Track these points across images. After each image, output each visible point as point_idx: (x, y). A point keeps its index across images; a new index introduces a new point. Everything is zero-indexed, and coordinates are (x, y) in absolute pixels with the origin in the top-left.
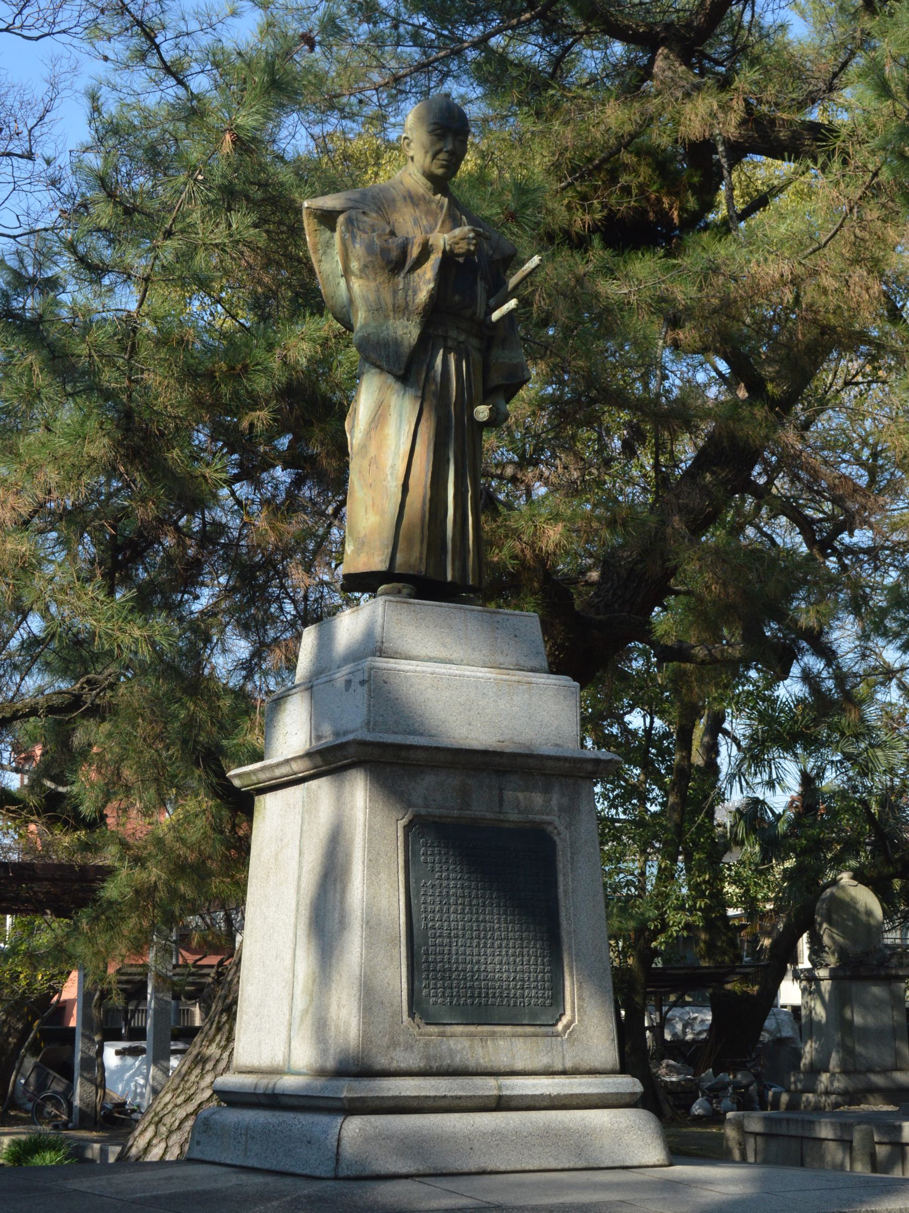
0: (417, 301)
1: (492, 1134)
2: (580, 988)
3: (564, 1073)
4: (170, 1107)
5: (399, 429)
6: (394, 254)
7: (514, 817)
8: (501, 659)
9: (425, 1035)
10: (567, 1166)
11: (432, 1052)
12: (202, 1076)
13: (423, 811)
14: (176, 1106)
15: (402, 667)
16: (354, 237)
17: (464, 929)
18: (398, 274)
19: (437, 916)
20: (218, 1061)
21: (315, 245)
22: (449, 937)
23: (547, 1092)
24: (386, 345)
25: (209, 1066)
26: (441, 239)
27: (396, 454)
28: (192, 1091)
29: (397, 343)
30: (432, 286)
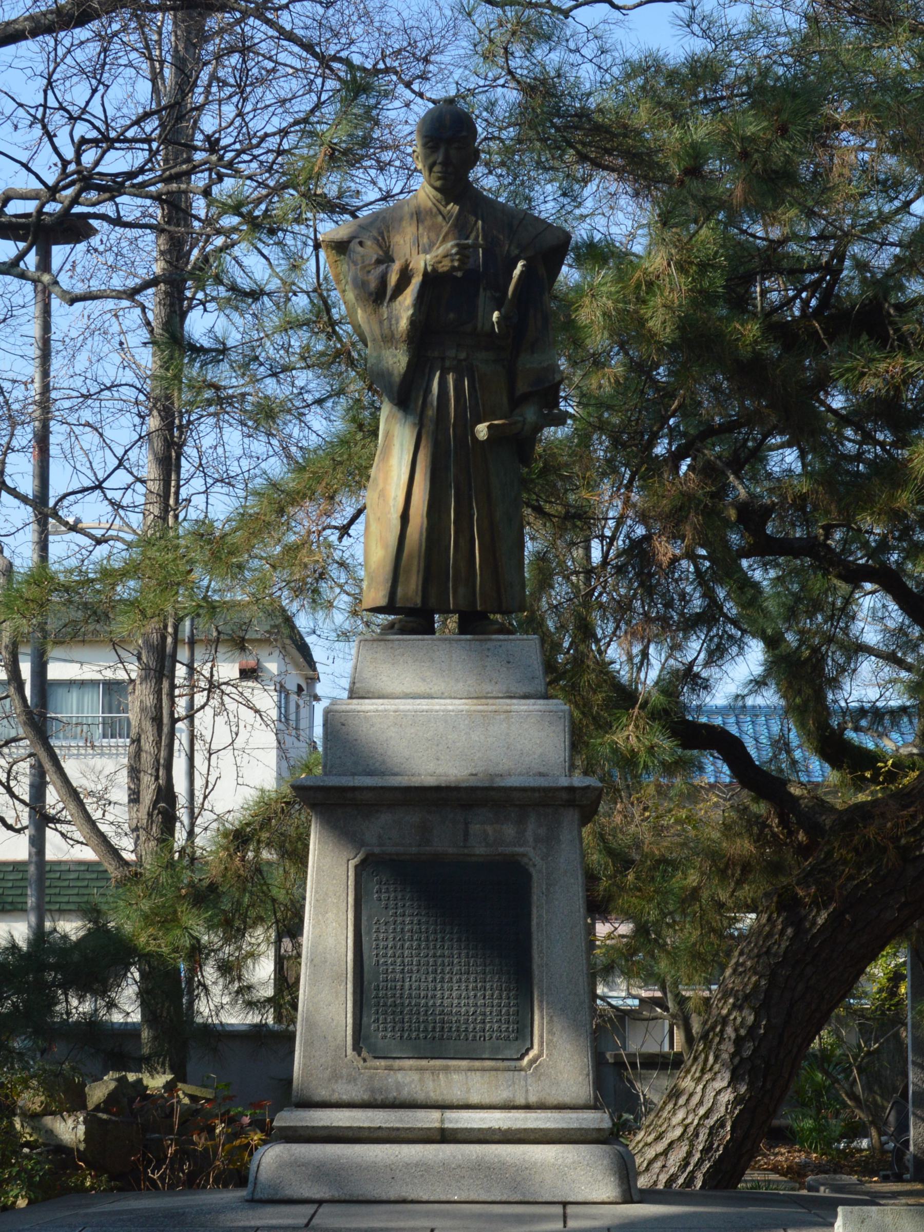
0: (400, 329)
1: (417, 1165)
2: (551, 1021)
3: (527, 1107)
4: (641, 1145)
5: (401, 459)
6: (373, 285)
7: (480, 850)
8: (488, 688)
9: (370, 1068)
10: (498, 1199)
11: (377, 1084)
12: (674, 1112)
13: (377, 850)
14: (646, 1144)
15: (363, 708)
17: (419, 965)
18: (382, 303)
19: (390, 952)
20: (691, 1095)
22: (402, 971)
23: (496, 1126)
25: (682, 1101)
28: (663, 1129)
30: (411, 312)
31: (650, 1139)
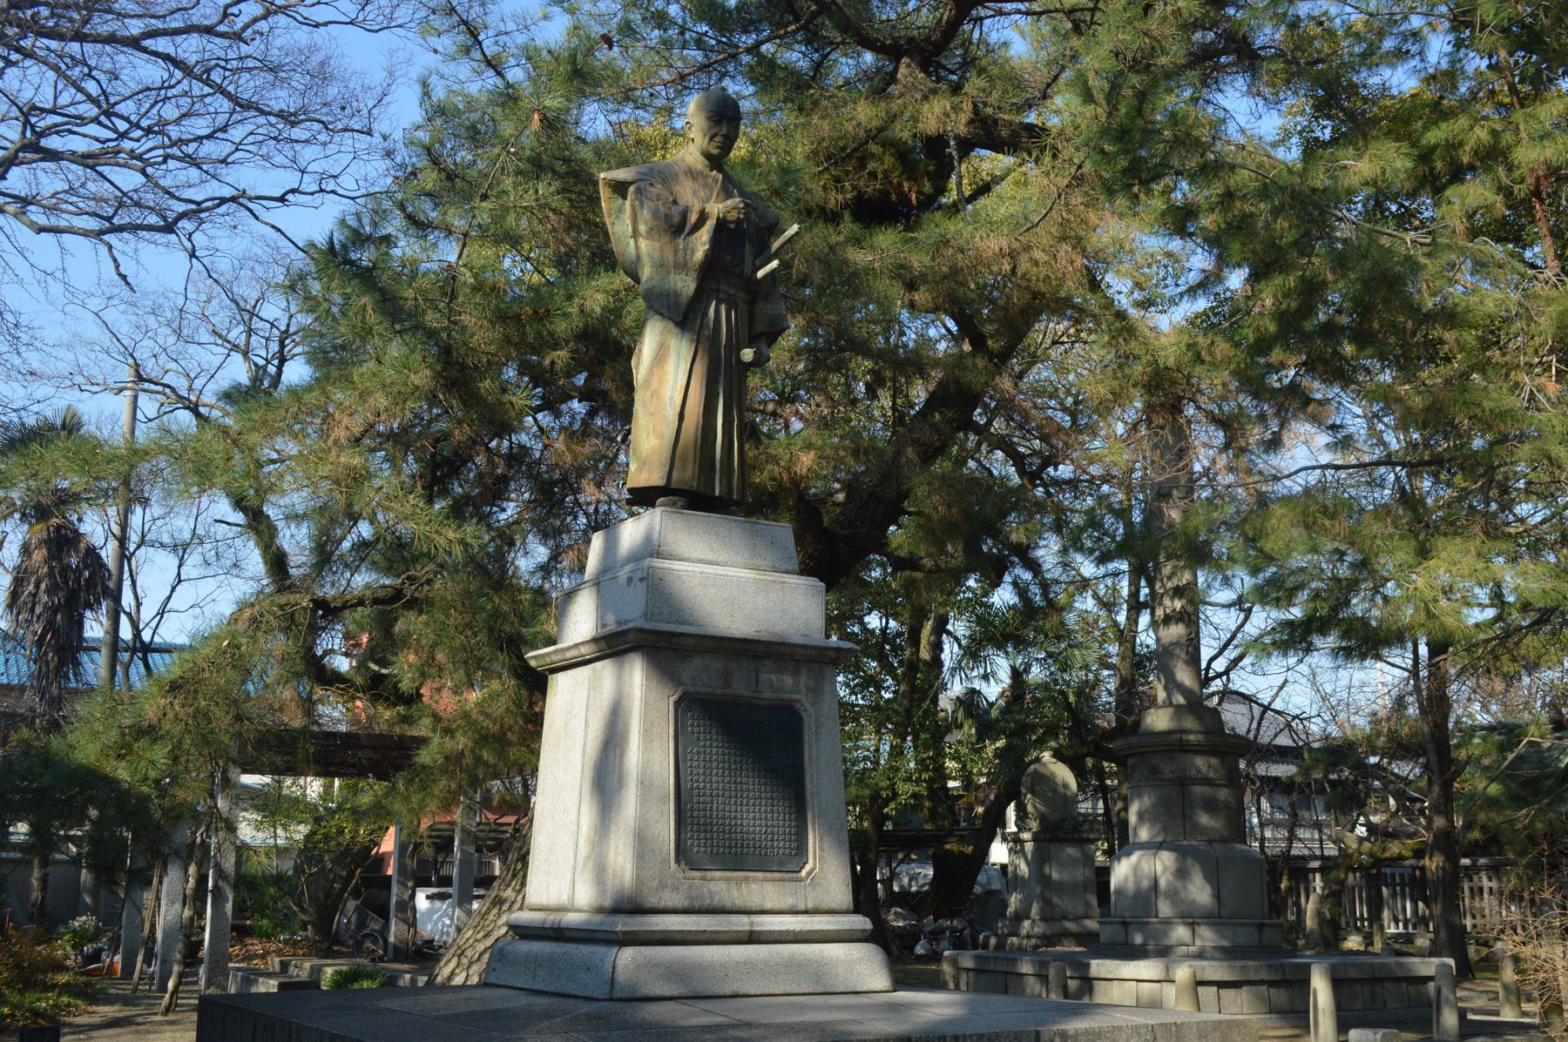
2: (821, 840)
6: (676, 220)
7: (767, 695)
8: (760, 562)
12: (499, 915)
13: (691, 689)
16: (642, 204)
21: (609, 210)
24: (668, 295)
25: (505, 907)
26: (716, 208)
27: (674, 388)
29: (677, 295)
31: (479, 936)
